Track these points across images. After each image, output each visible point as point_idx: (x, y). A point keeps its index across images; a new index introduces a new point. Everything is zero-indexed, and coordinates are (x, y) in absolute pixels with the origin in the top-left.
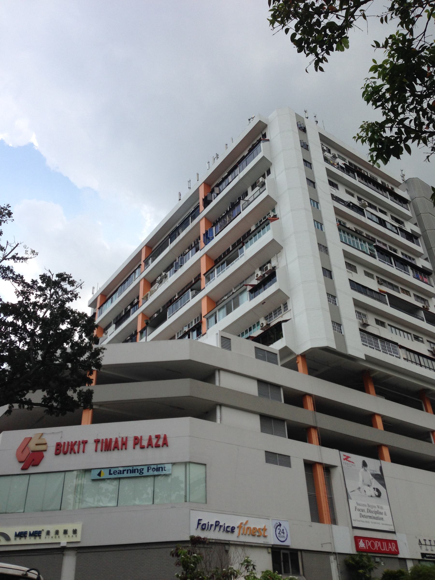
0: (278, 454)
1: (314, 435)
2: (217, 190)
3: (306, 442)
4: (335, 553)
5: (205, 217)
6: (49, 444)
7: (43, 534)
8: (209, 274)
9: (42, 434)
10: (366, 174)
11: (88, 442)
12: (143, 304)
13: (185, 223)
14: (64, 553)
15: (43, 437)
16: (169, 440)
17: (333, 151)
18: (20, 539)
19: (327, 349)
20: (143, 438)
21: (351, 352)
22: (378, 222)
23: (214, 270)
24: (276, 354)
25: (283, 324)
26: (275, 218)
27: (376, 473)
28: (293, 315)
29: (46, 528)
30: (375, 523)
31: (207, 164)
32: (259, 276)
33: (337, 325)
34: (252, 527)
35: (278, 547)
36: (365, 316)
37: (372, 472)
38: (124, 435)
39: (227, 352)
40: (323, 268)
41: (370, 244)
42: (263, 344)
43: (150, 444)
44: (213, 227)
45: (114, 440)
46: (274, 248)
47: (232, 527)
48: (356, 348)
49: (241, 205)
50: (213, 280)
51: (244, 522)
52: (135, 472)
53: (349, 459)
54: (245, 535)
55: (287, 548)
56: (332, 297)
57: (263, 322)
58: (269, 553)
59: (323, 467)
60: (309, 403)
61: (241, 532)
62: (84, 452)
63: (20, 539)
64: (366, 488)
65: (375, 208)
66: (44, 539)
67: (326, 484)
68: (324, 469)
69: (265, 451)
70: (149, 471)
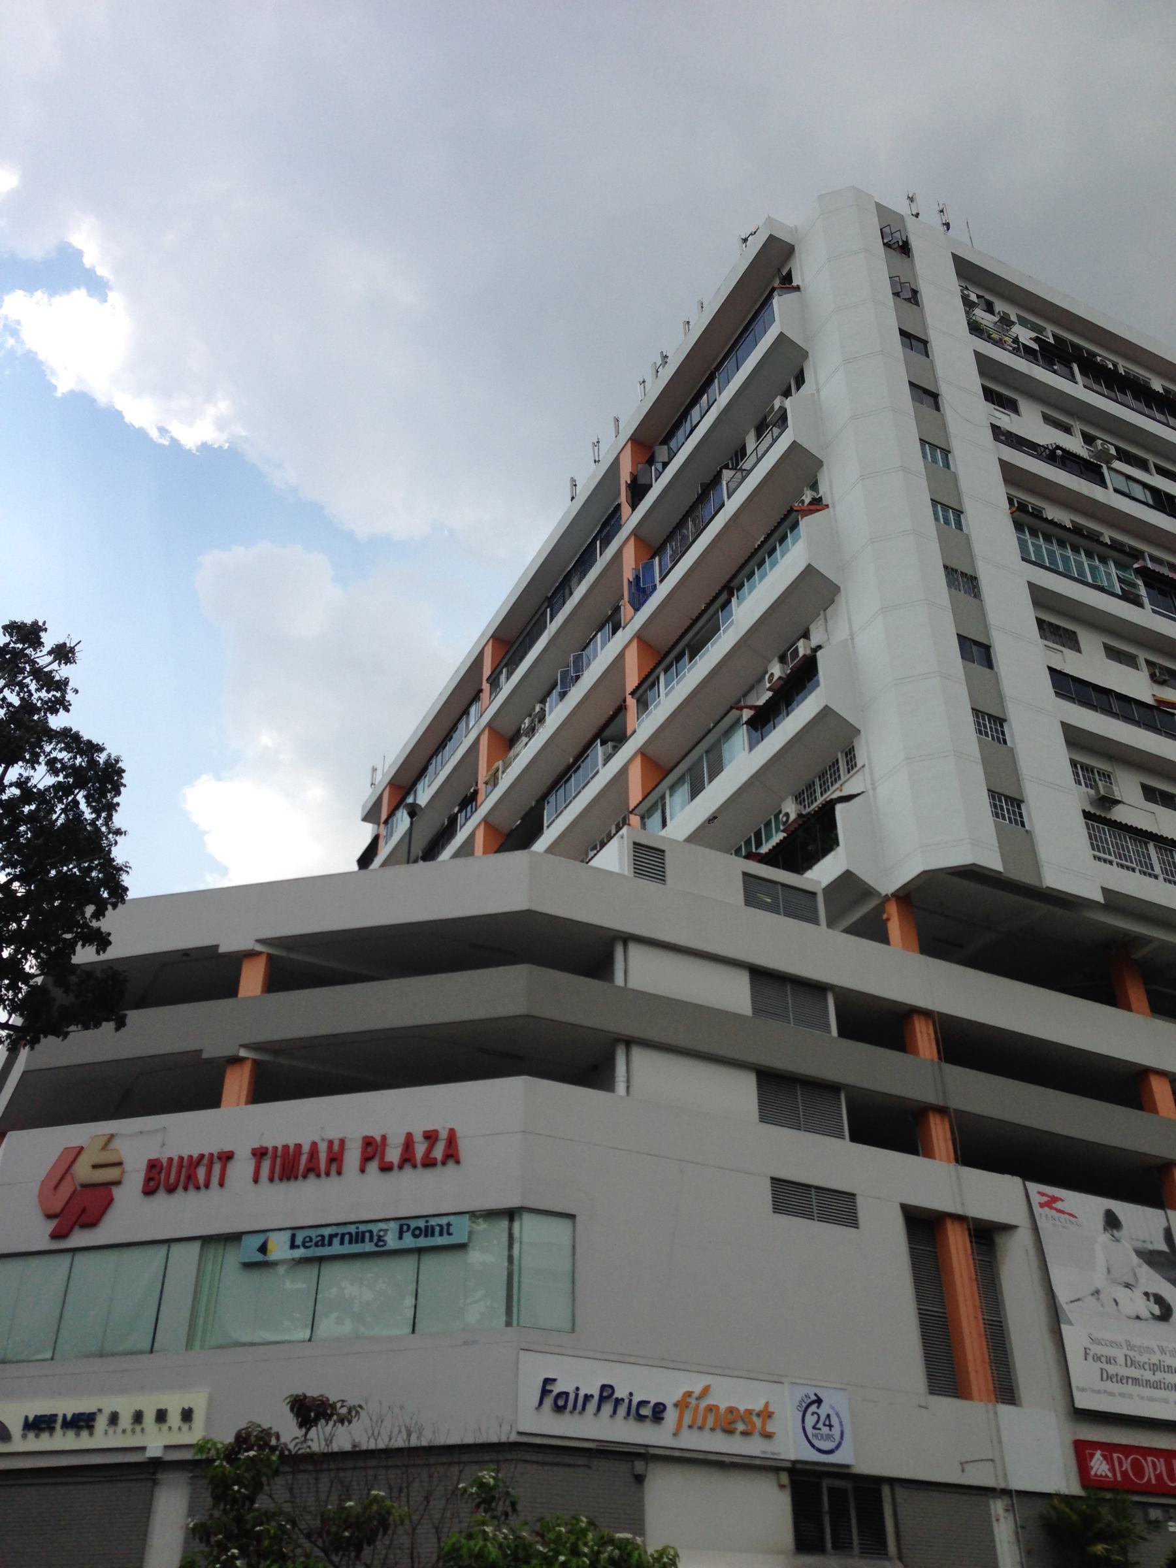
0: (817, 1188)
1: (940, 1132)
2: (662, 453)
4: (1006, 1493)
5: (635, 533)
6: (127, 1166)
7: (101, 1423)
8: (645, 692)
9: (112, 1136)
10: (1111, 366)
11: (236, 1157)
12: (487, 797)
13: (585, 561)
14: (158, 1476)
15: (116, 1144)
16: (465, 1148)
17: (1000, 306)
18: (37, 1436)
19: (971, 873)
20: (390, 1141)
21: (1055, 878)
22: (1151, 502)
23: (658, 678)
24: (814, 894)
25: (839, 808)
26: (818, 504)
27: (1150, 1247)
28: (872, 779)
29: (108, 1404)
30: (1151, 1399)
31: (639, 388)
32: (776, 677)
33: (1008, 804)
34: (723, 1406)
35: (808, 1467)
36: (1106, 776)
37: (1139, 1245)
38: (335, 1134)
39: (651, 886)
40: (961, 638)
41: (1119, 565)
42: (785, 868)
43: (407, 1158)
44: (653, 557)
45: (306, 1149)
46: (815, 593)
47: (657, 1404)
48: (1070, 864)
49: (724, 483)
50: (655, 707)
51: (697, 1390)
52: (363, 1241)
53: (1058, 1205)
54: (700, 1428)
55: (841, 1473)
56: (991, 723)
57: (791, 809)
58: (782, 1486)
59: (969, 1230)
60: (924, 1037)
61: (687, 1420)
62: (221, 1184)
63: (37, 1436)
64: (1122, 1294)
65: (1142, 465)
66: (101, 1438)
67: (977, 1280)
68: (970, 1235)
69: (772, 1178)
70: (405, 1235)
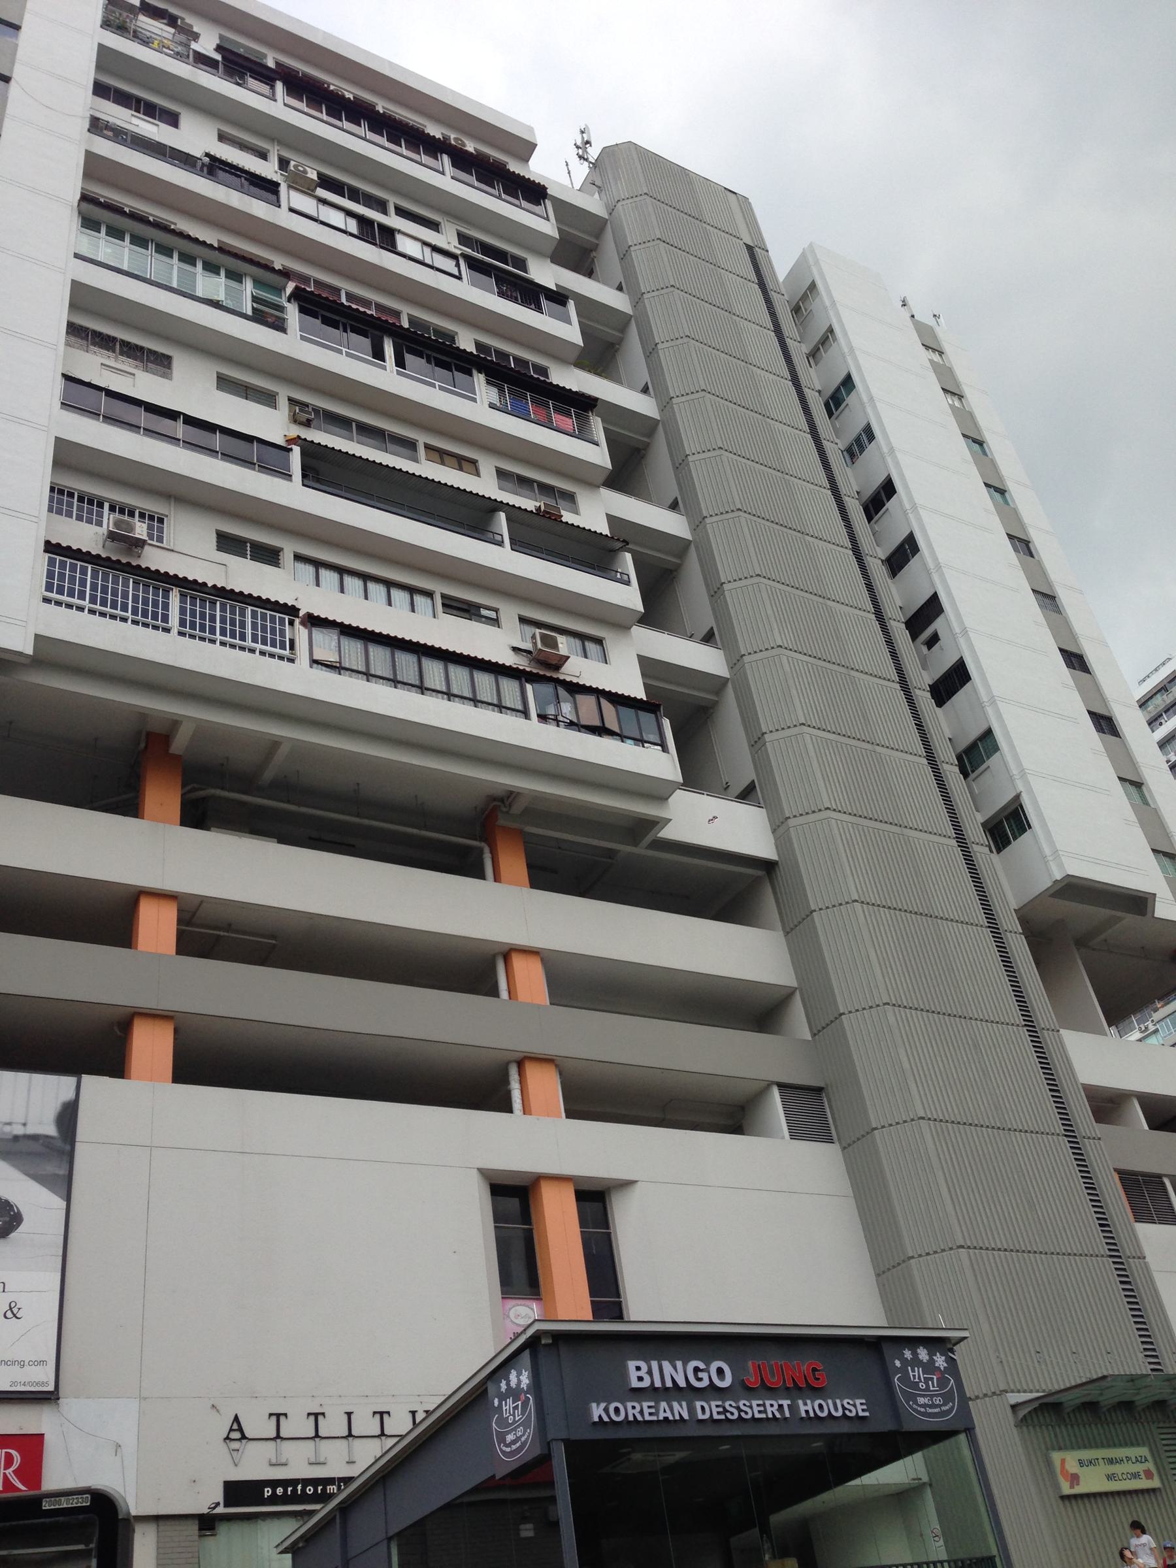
3: (743, 1134)
22: (355, 231)
60: (157, 927)
